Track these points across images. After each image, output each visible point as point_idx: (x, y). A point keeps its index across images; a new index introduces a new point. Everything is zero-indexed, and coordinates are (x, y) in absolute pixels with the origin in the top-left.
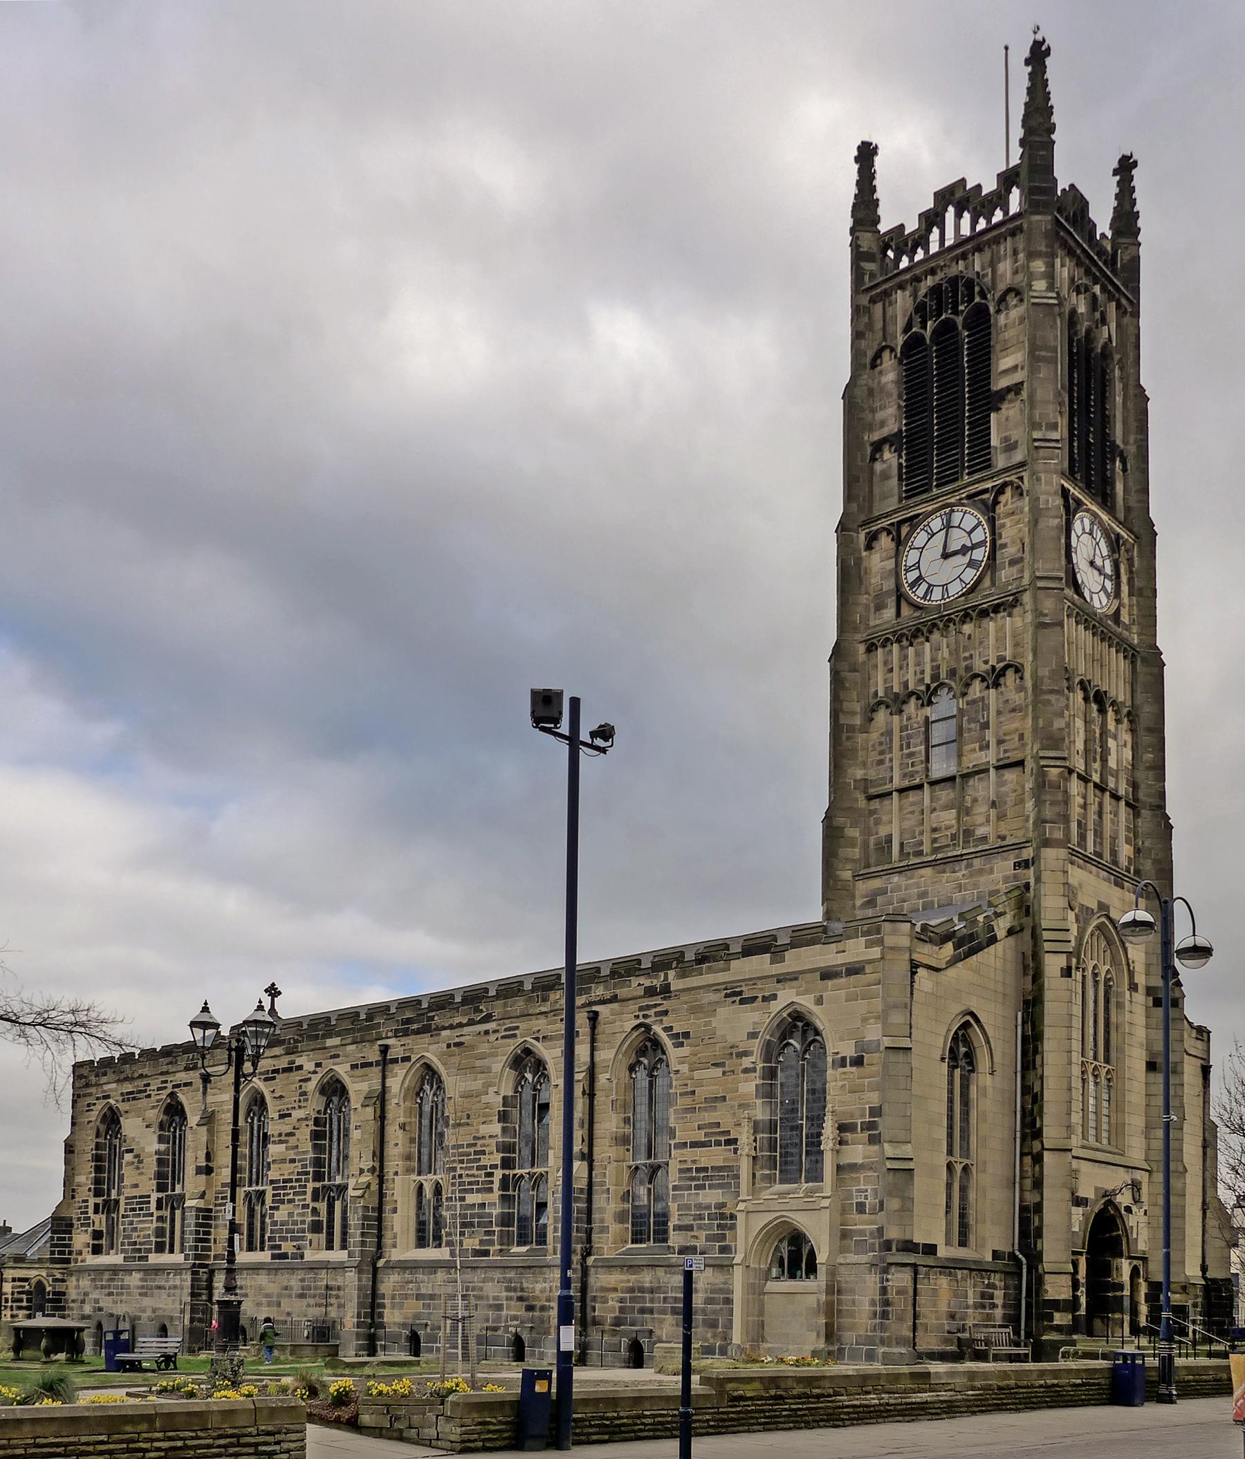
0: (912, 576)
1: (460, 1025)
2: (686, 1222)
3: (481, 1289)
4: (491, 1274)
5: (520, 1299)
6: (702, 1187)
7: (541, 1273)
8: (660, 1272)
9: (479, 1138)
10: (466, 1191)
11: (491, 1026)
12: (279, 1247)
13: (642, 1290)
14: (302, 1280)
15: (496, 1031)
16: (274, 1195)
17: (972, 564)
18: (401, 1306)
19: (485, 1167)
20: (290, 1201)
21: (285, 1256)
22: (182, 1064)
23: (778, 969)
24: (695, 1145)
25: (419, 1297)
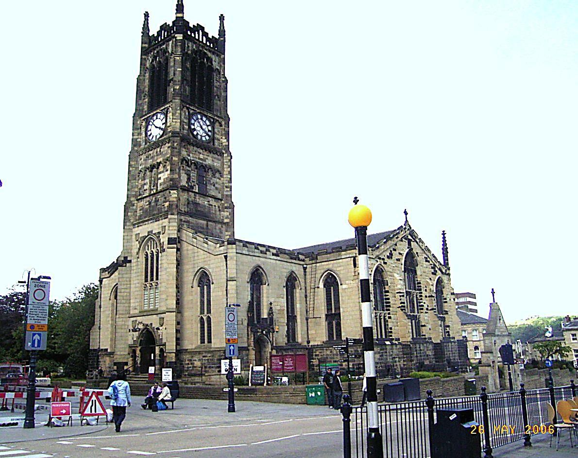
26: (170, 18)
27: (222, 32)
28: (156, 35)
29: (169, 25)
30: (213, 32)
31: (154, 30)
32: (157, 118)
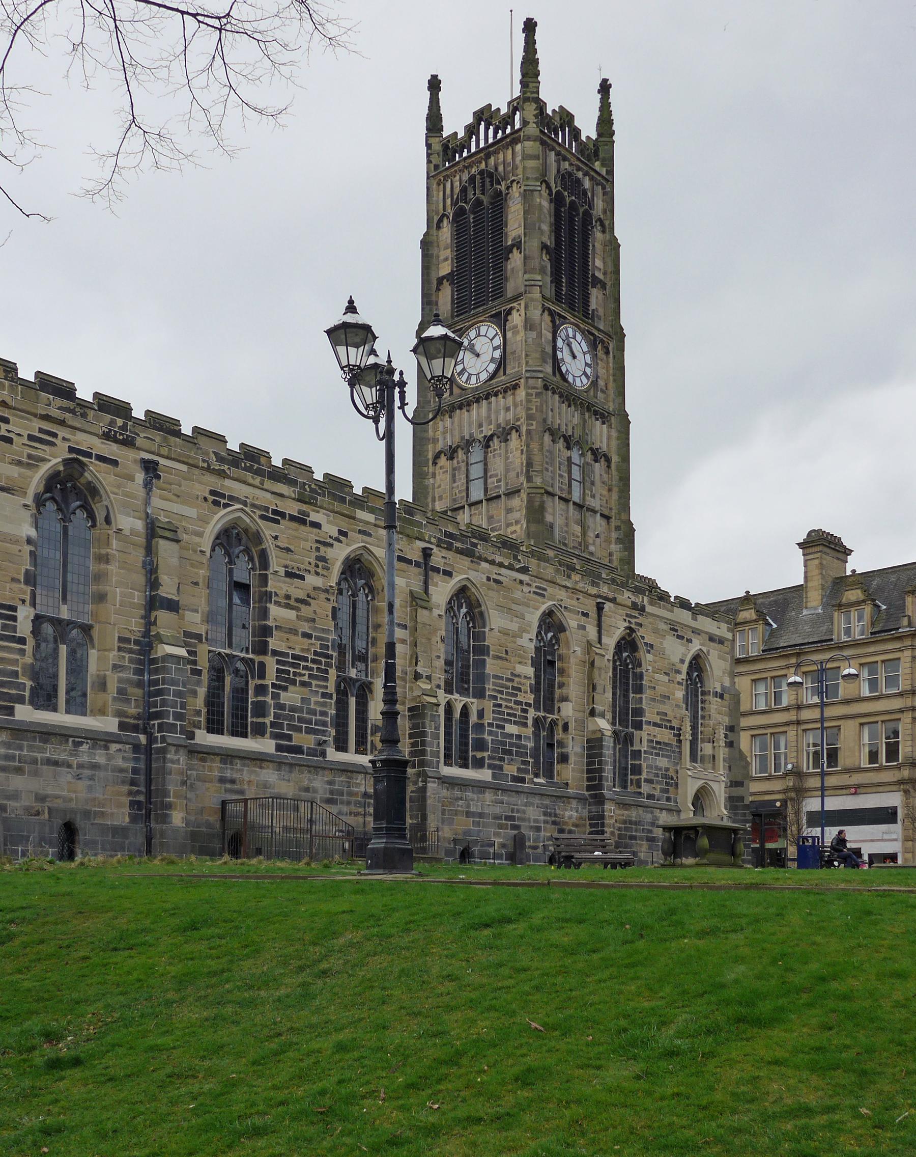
1: (501, 565)
2: (651, 777)
3: (524, 812)
4: (531, 800)
5: (554, 823)
6: (657, 755)
7: (569, 803)
8: (641, 810)
9: (515, 676)
10: (505, 720)
11: (525, 578)
12: (289, 738)
13: (631, 822)
14: (331, 783)
15: (528, 585)
16: (278, 670)
18: (451, 821)
19: (520, 703)
20: (303, 684)
21: (298, 750)
22: (102, 427)
23: (693, 624)
24: (655, 724)
25: (468, 814)
26: (501, 93)
27: (605, 122)
28: (461, 134)
29: (498, 110)
30: (588, 129)
31: (455, 122)
32: (585, 373)
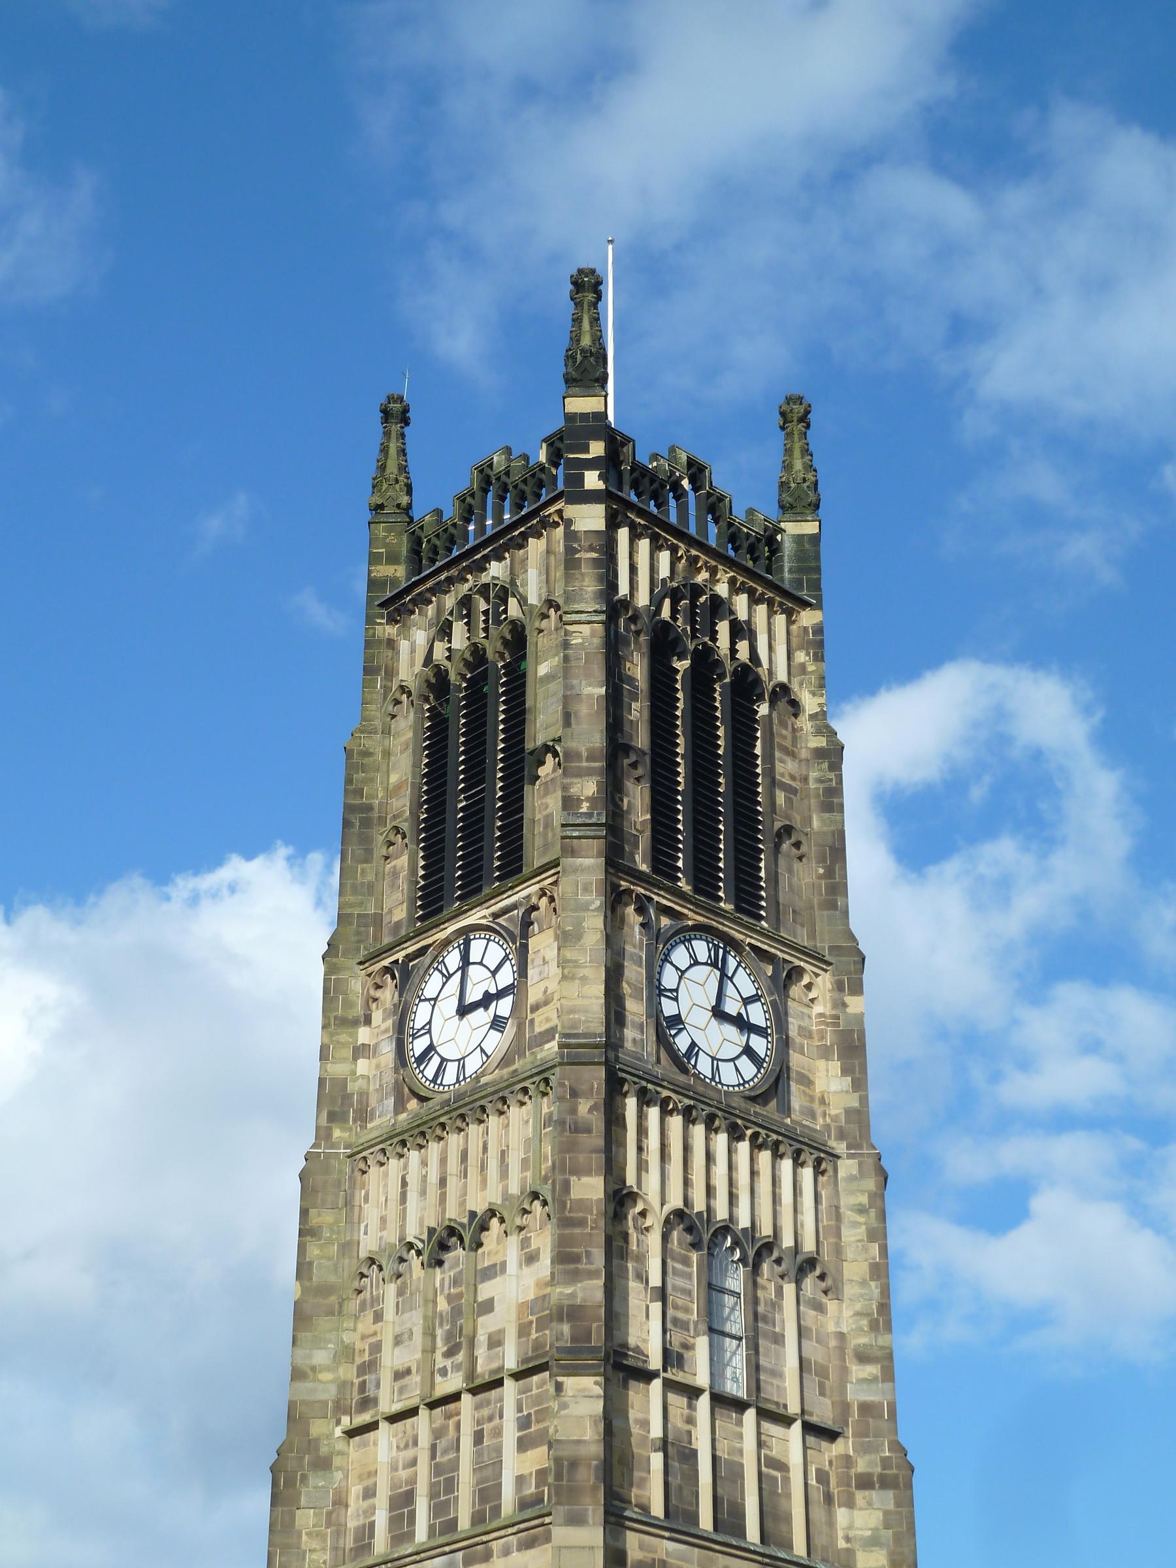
0: (420, 1045)
17: (497, 1023)
